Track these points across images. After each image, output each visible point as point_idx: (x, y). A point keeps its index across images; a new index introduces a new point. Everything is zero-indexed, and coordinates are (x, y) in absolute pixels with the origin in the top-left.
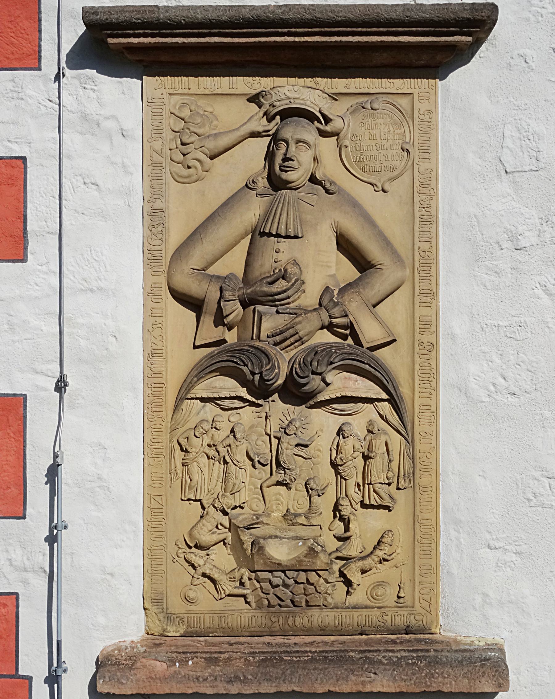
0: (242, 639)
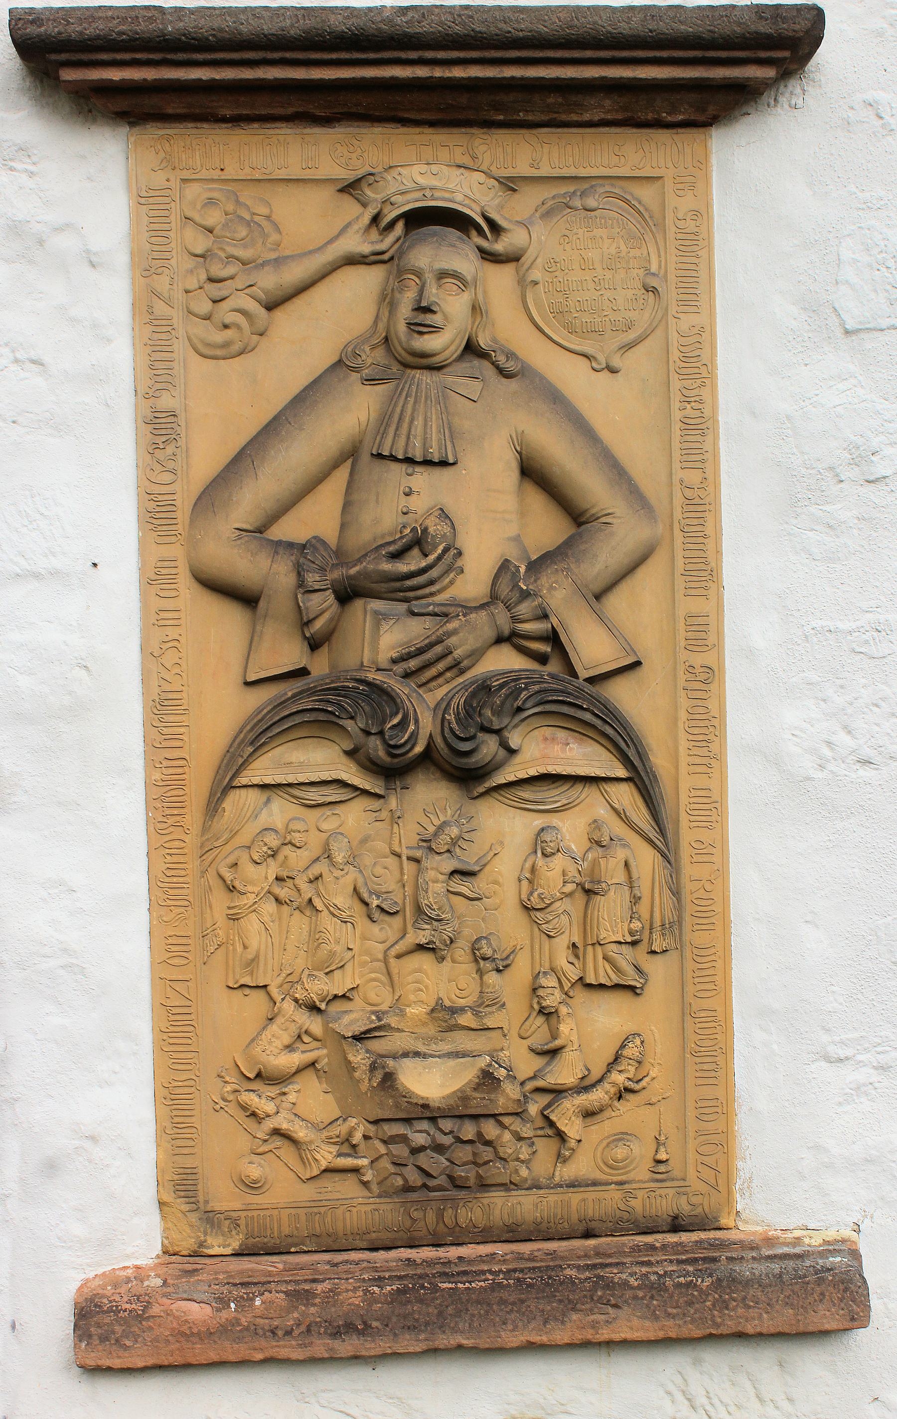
0: (354, 1256)
